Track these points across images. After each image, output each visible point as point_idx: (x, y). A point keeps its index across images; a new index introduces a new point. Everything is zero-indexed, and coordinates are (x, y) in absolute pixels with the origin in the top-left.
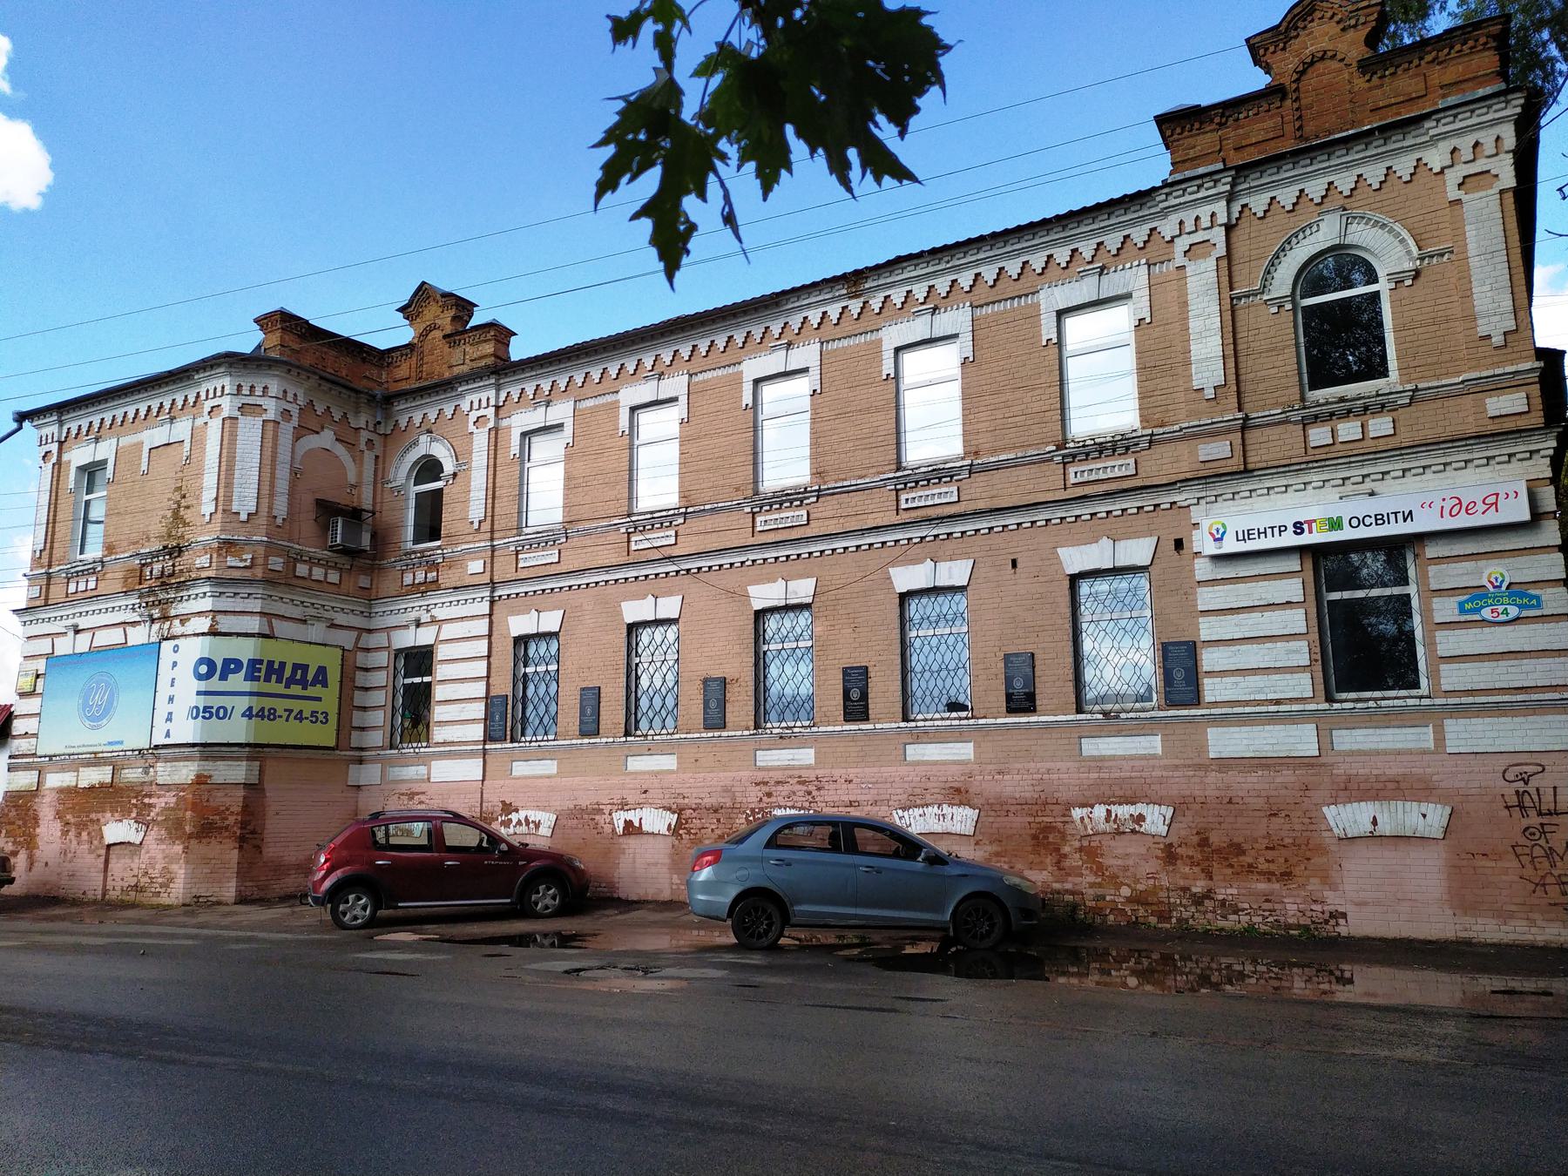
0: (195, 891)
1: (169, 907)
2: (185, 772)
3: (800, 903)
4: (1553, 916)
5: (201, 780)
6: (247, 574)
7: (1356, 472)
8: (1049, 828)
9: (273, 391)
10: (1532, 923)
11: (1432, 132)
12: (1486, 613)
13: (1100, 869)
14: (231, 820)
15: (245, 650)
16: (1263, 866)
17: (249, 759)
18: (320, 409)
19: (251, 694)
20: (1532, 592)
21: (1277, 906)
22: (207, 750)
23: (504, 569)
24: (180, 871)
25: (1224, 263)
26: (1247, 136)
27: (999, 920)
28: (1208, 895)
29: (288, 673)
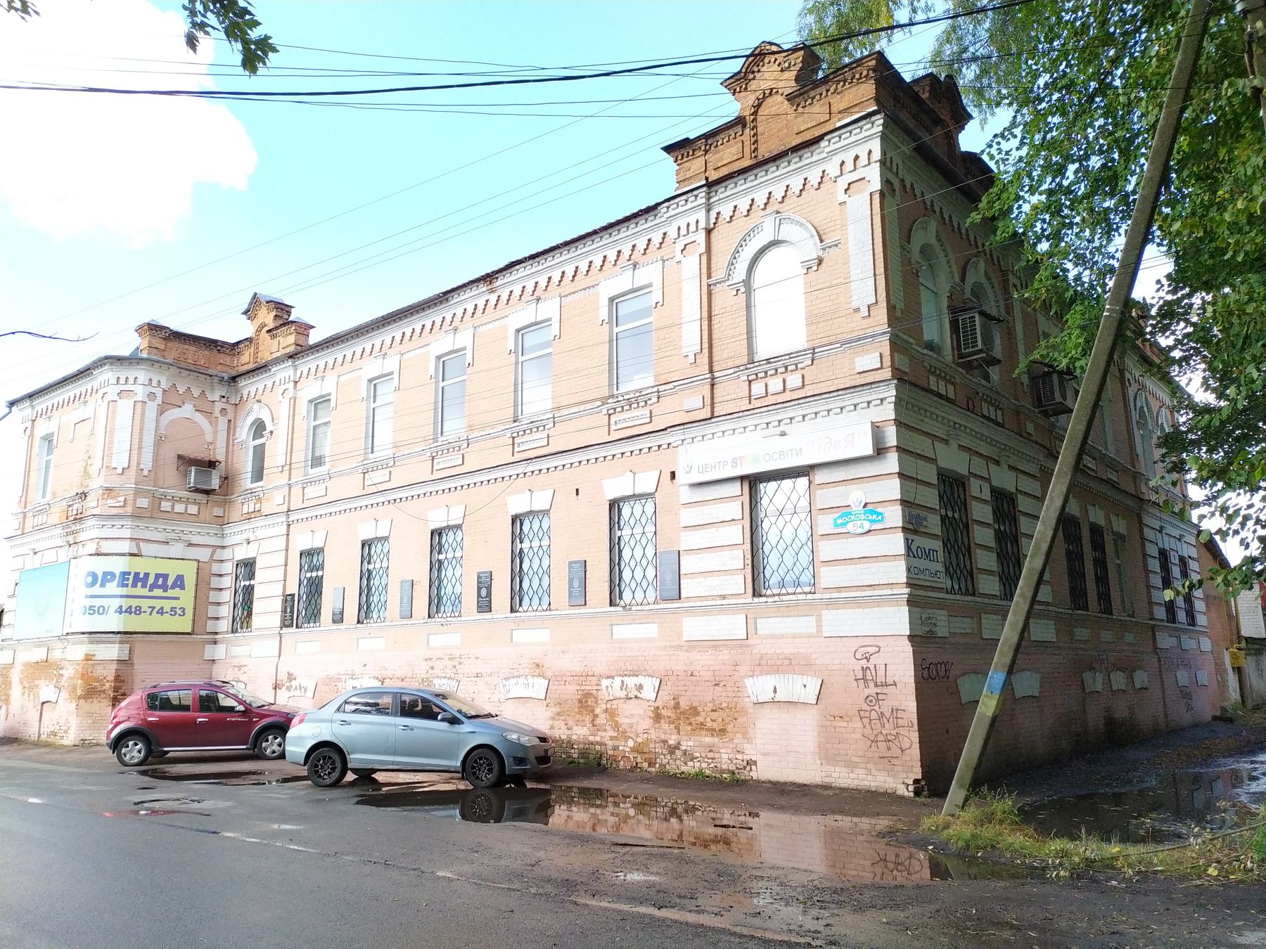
0: (82, 736)
1: (62, 746)
2: (78, 651)
3: (353, 753)
4: (881, 766)
5: (88, 658)
6: (121, 511)
7: (774, 418)
8: (588, 695)
9: (140, 381)
10: (869, 772)
11: (827, 150)
12: (850, 527)
13: (616, 726)
14: (107, 685)
15: (119, 565)
16: (709, 724)
17: (121, 642)
18: (181, 389)
19: (122, 596)
20: (879, 510)
21: (717, 755)
22: (94, 636)
23: (296, 503)
24: (74, 722)
25: (704, 258)
26: (719, 160)
27: (496, 766)
28: (677, 747)
29: (151, 580)
